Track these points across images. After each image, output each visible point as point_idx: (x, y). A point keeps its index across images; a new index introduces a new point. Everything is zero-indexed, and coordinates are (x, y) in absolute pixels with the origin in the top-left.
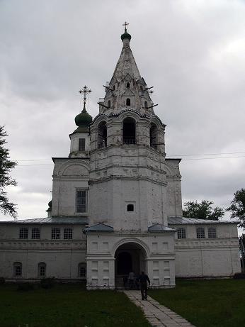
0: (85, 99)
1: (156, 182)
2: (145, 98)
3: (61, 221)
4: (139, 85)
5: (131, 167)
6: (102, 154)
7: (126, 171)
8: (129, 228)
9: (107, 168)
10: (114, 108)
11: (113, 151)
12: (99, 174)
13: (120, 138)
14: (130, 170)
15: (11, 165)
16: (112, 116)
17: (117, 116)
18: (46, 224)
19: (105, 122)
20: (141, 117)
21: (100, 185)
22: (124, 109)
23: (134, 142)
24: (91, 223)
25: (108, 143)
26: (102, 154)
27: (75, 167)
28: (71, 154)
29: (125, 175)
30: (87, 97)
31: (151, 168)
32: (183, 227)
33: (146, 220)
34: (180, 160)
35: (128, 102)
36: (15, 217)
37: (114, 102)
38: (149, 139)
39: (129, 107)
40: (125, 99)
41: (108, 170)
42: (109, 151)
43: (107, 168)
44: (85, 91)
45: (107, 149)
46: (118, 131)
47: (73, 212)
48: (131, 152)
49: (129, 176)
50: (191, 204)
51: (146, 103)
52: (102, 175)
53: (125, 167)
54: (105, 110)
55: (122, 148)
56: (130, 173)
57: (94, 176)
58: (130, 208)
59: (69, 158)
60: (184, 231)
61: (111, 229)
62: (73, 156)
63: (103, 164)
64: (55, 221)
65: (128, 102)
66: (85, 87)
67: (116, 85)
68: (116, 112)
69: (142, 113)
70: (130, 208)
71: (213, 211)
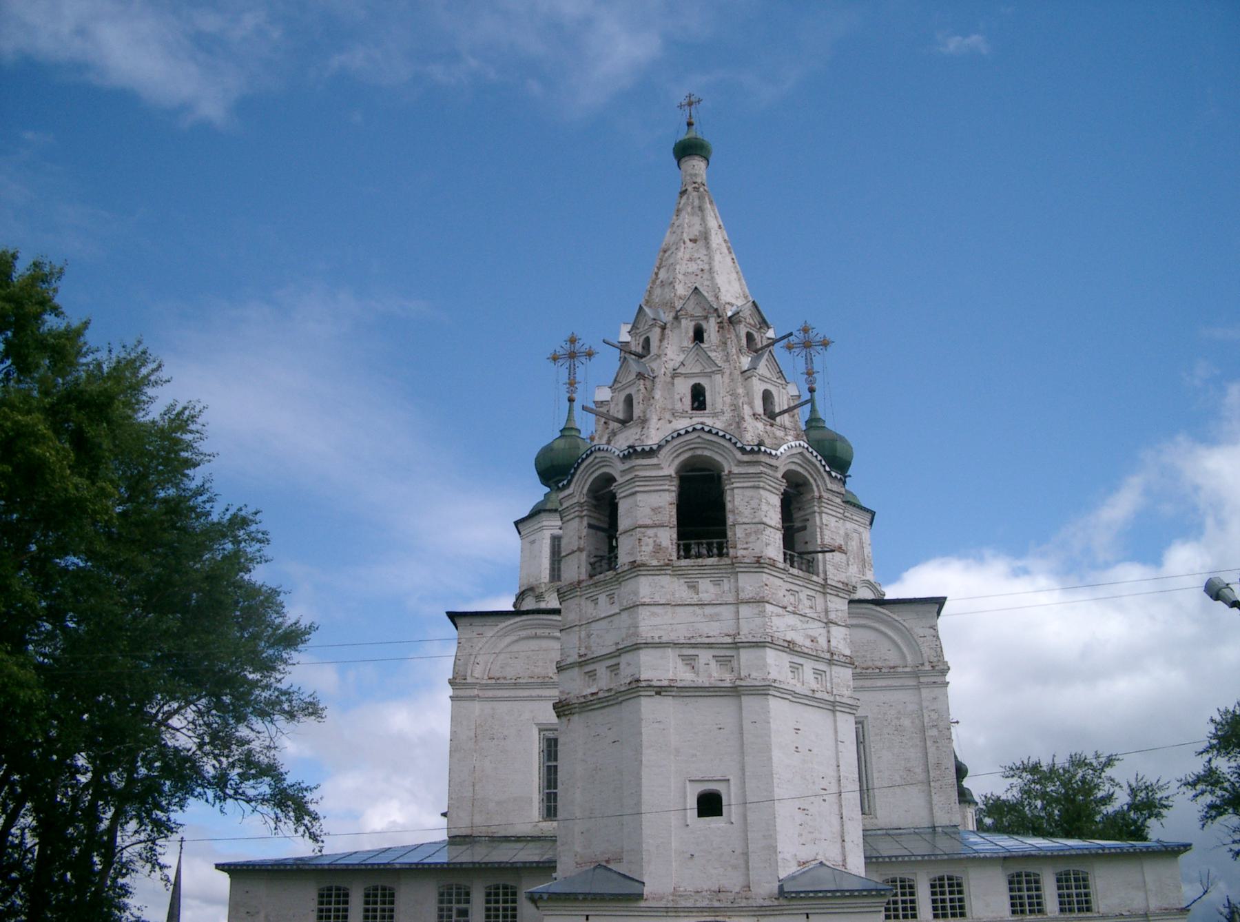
0: (810, 373)
1: (809, 700)
2: (762, 379)
3: (479, 854)
4: (743, 330)
5: (710, 646)
6: (603, 599)
7: (690, 661)
8: (706, 886)
9: (620, 652)
10: (644, 421)
11: (645, 587)
12: (592, 675)
13: (668, 537)
14: (705, 656)
15: (293, 638)
16: (632, 453)
17: (651, 453)
18: (419, 871)
19: (610, 479)
20: (743, 450)
21: (598, 717)
22: (682, 424)
23: (720, 547)
24: (566, 868)
25: (623, 558)
26: (603, 599)
27: (534, 644)
28: (521, 596)
29: (685, 676)
30: (579, 376)
31: (790, 647)
32: (1031, 869)
33: (773, 849)
34: (939, 602)
35: (698, 398)
36: (314, 837)
37: (649, 398)
38: (779, 536)
39: (698, 419)
40: (683, 388)
41: (624, 659)
42: (626, 588)
43: (620, 652)
44: (573, 354)
45: (619, 579)
46: (655, 510)
47: (530, 818)
48: (707, 589)
49: (703, 680)
50: (1035, 769)
51: (767, 397)
52: (604, 680)
53: (688, 648)
54: (614, 434)
55: (677, 573)
56: (710, 671)
57: (577, 686)
58: (710, 805)
59: (517, 613)
60: (956, 886)
61: (633, 888)
62: (529, 604)
63: (604, 640)
64: (465, 856)
65: (698, 398)
66: (573, 341)
67: (655, 335)
68: (653, 437)
69: (750, 438)
70: (710, 805)
71: (1122, 799)
